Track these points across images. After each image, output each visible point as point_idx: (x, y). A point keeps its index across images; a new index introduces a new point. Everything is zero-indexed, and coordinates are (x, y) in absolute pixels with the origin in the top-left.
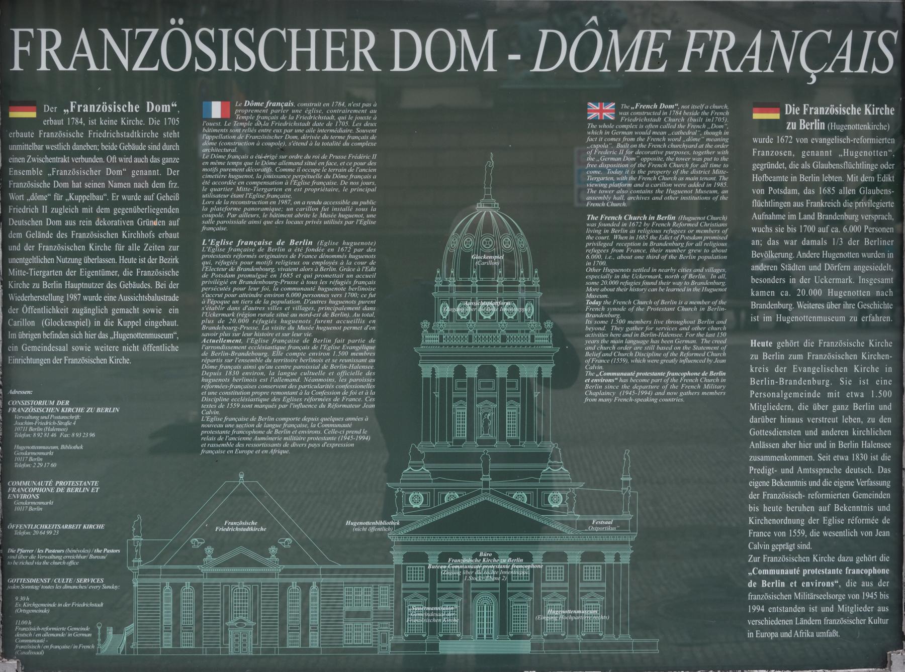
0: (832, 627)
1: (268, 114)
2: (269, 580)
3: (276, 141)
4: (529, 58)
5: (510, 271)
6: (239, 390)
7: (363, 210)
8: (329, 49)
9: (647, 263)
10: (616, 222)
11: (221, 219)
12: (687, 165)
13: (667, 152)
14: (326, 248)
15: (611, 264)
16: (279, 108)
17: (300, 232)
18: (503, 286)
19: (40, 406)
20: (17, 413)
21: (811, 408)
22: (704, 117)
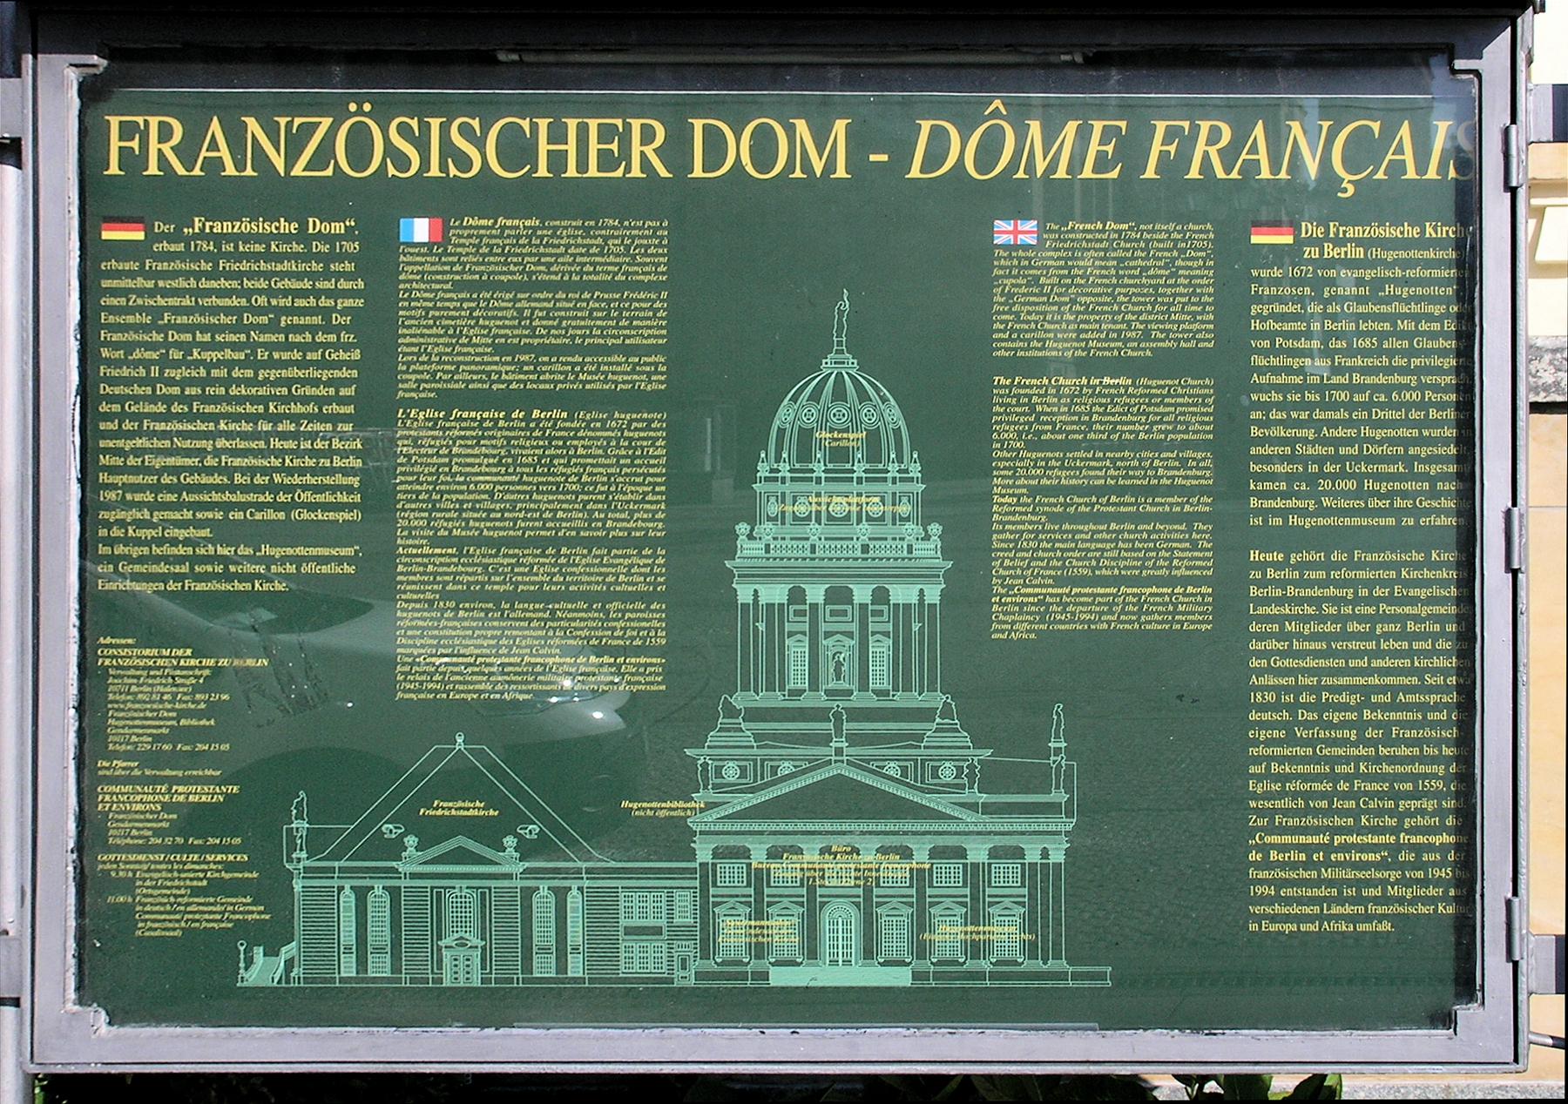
0: (1381, 918)
1: (500, 236)
2: (506, 883)
3: (513, 273)
4: (902, 157)
5: (874, 454)
6: (455, 628)
7: (648, 369)
8: (594, 146)
9: (1091, 446)
10: (1040, 387)
11: (426, 382)
12: (1149, 308)
13: (1118, 290)
14: (589, 423)
15: (1031, 446)
16: (518, 227)
17: (548, 400)
18: (864, 475)
19: (148, 657)
20: (112, 666)
21: (1344, 628)
22: (1176, 241)
